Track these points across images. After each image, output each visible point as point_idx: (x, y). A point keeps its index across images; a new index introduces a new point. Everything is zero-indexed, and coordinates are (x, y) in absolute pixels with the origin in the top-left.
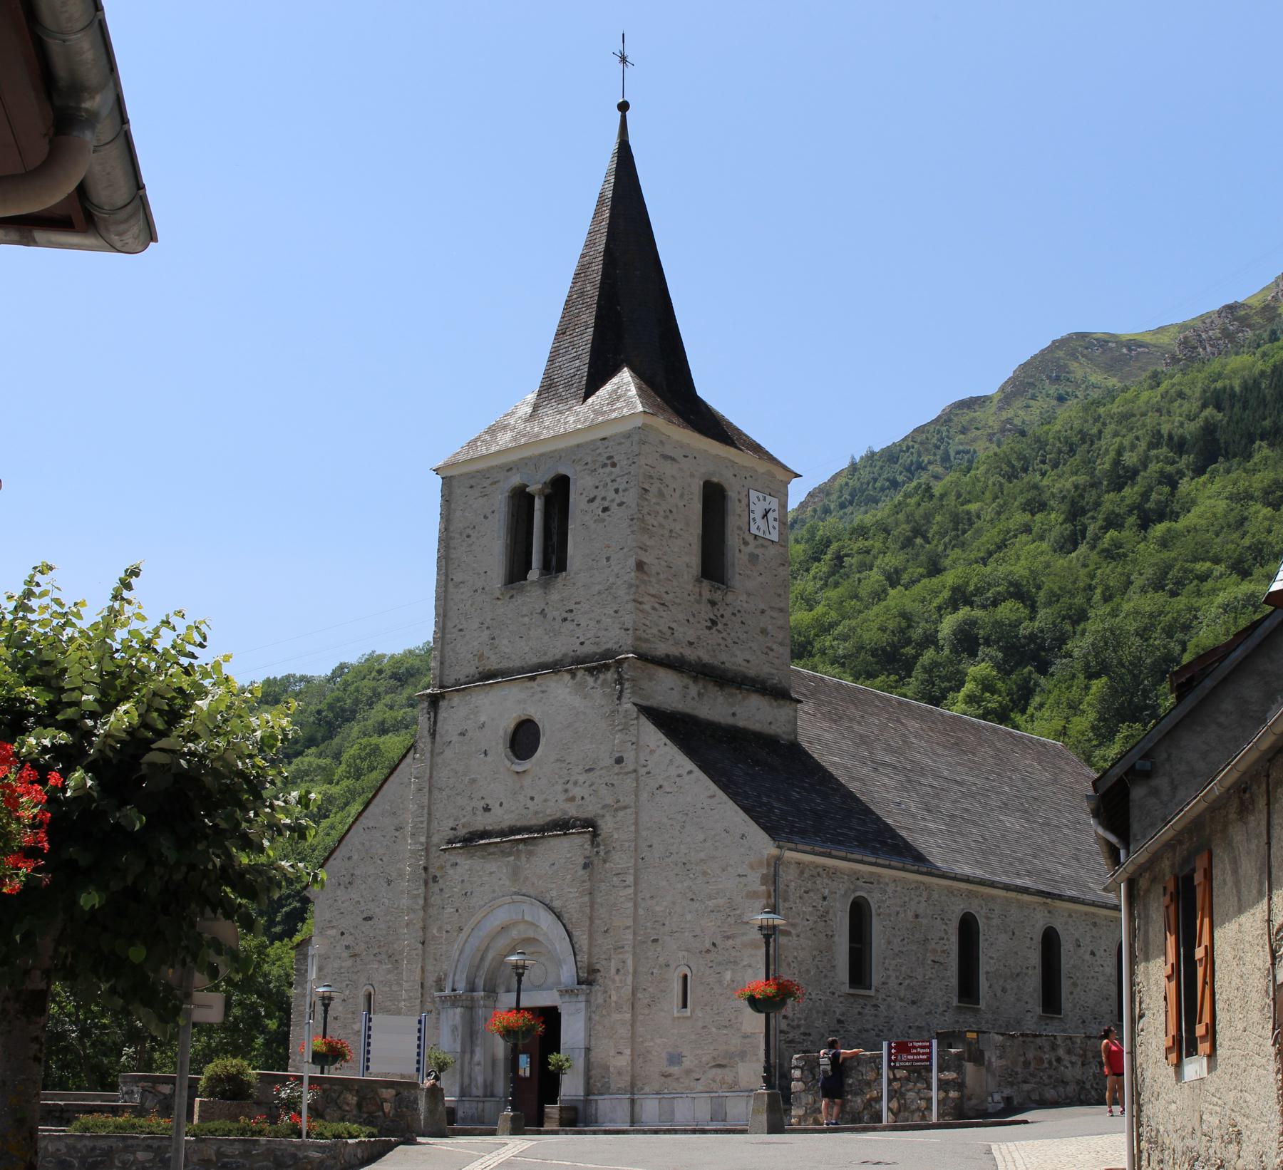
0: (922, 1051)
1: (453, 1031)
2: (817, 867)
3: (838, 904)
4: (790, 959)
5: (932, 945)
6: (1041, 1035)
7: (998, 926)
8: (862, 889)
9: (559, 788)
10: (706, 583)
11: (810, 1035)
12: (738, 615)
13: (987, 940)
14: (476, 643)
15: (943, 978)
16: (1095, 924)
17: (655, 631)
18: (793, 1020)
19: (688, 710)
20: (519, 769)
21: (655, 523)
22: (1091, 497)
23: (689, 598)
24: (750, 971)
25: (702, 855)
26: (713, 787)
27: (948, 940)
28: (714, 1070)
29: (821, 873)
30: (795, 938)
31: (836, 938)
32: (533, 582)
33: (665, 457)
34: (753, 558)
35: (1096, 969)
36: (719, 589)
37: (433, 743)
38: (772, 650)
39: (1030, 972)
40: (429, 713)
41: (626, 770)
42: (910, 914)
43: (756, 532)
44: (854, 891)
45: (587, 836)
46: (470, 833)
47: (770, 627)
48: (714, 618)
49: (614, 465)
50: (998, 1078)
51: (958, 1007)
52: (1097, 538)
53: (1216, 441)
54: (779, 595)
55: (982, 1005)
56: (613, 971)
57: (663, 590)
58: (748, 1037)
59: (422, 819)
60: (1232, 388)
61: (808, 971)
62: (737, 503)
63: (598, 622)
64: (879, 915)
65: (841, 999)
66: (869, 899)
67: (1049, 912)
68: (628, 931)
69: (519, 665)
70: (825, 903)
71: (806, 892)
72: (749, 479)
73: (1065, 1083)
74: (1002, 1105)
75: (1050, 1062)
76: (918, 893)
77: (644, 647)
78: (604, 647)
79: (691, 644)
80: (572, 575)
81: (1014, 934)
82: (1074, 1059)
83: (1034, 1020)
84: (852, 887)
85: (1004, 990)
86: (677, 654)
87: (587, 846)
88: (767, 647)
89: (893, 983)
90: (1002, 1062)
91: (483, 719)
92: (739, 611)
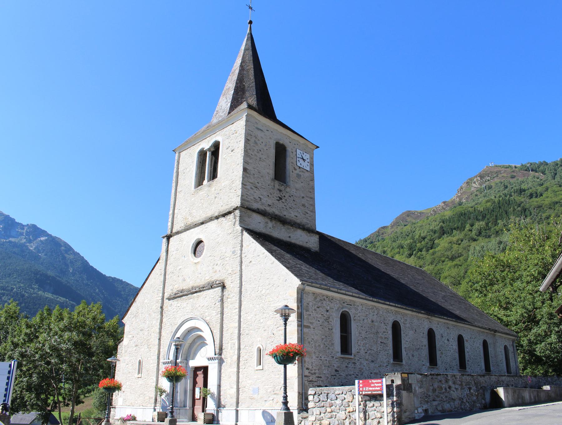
0: (377, 385)
2: (323, 296)
3: (334, 314)
4: (310, 340)
5: (380, 335)
6: (440, 375)
7: (409, 327)
8: (346, 307)
10: (276, 182)
11: (321, 377)
12: (292, 197)
13: (404, 333)
14: (184, 214)
15: (386, 350)
16: (448, 328)
17: (252, 198)
19: (267, 233)
21: (253, 154)
22: (414, 244)
23: (268, 187)
26: (273, 259)
27: (387, 333)
30: (312, 329)
31: (334, 330)
33: (258, 129)
34: (299, 176)
35: (450, 347)
36: (283, 185)
38: (308, 213)
39: (423, 348)
42: (370, 321)
43: (300, 166)
44: (342, 308)
45: (220, 288)
47: (306, 204)
48: (281, 197)
50: (420, 399)
51: (393, 363)
52: (416, 254)
53: (444, 230)
54: (310, 192)
55: (404, 362)
57: (256, 182)
60: (446, 218)
61: (319, 346)
62: (291, 153)
64: (355, 320)
65: (337, 360)
66: (350, 313)
67: (430, 322)
70: (328, 313)
71: (318, 308)
72: (296, 145)
73: (454, 400)
74: (423, 414)
75: (446, 389)
76: (372, 311)
77: (247, 204)
79: (269, 205)
81: (416, 331)
82: (457, 386)
83: (426, 369)
84: (341, 306)
85: (413, 356)
86: (263, 209)
88: (305, 212)
89: (362, 352)
90: (421, 390)
92: (292, 196)
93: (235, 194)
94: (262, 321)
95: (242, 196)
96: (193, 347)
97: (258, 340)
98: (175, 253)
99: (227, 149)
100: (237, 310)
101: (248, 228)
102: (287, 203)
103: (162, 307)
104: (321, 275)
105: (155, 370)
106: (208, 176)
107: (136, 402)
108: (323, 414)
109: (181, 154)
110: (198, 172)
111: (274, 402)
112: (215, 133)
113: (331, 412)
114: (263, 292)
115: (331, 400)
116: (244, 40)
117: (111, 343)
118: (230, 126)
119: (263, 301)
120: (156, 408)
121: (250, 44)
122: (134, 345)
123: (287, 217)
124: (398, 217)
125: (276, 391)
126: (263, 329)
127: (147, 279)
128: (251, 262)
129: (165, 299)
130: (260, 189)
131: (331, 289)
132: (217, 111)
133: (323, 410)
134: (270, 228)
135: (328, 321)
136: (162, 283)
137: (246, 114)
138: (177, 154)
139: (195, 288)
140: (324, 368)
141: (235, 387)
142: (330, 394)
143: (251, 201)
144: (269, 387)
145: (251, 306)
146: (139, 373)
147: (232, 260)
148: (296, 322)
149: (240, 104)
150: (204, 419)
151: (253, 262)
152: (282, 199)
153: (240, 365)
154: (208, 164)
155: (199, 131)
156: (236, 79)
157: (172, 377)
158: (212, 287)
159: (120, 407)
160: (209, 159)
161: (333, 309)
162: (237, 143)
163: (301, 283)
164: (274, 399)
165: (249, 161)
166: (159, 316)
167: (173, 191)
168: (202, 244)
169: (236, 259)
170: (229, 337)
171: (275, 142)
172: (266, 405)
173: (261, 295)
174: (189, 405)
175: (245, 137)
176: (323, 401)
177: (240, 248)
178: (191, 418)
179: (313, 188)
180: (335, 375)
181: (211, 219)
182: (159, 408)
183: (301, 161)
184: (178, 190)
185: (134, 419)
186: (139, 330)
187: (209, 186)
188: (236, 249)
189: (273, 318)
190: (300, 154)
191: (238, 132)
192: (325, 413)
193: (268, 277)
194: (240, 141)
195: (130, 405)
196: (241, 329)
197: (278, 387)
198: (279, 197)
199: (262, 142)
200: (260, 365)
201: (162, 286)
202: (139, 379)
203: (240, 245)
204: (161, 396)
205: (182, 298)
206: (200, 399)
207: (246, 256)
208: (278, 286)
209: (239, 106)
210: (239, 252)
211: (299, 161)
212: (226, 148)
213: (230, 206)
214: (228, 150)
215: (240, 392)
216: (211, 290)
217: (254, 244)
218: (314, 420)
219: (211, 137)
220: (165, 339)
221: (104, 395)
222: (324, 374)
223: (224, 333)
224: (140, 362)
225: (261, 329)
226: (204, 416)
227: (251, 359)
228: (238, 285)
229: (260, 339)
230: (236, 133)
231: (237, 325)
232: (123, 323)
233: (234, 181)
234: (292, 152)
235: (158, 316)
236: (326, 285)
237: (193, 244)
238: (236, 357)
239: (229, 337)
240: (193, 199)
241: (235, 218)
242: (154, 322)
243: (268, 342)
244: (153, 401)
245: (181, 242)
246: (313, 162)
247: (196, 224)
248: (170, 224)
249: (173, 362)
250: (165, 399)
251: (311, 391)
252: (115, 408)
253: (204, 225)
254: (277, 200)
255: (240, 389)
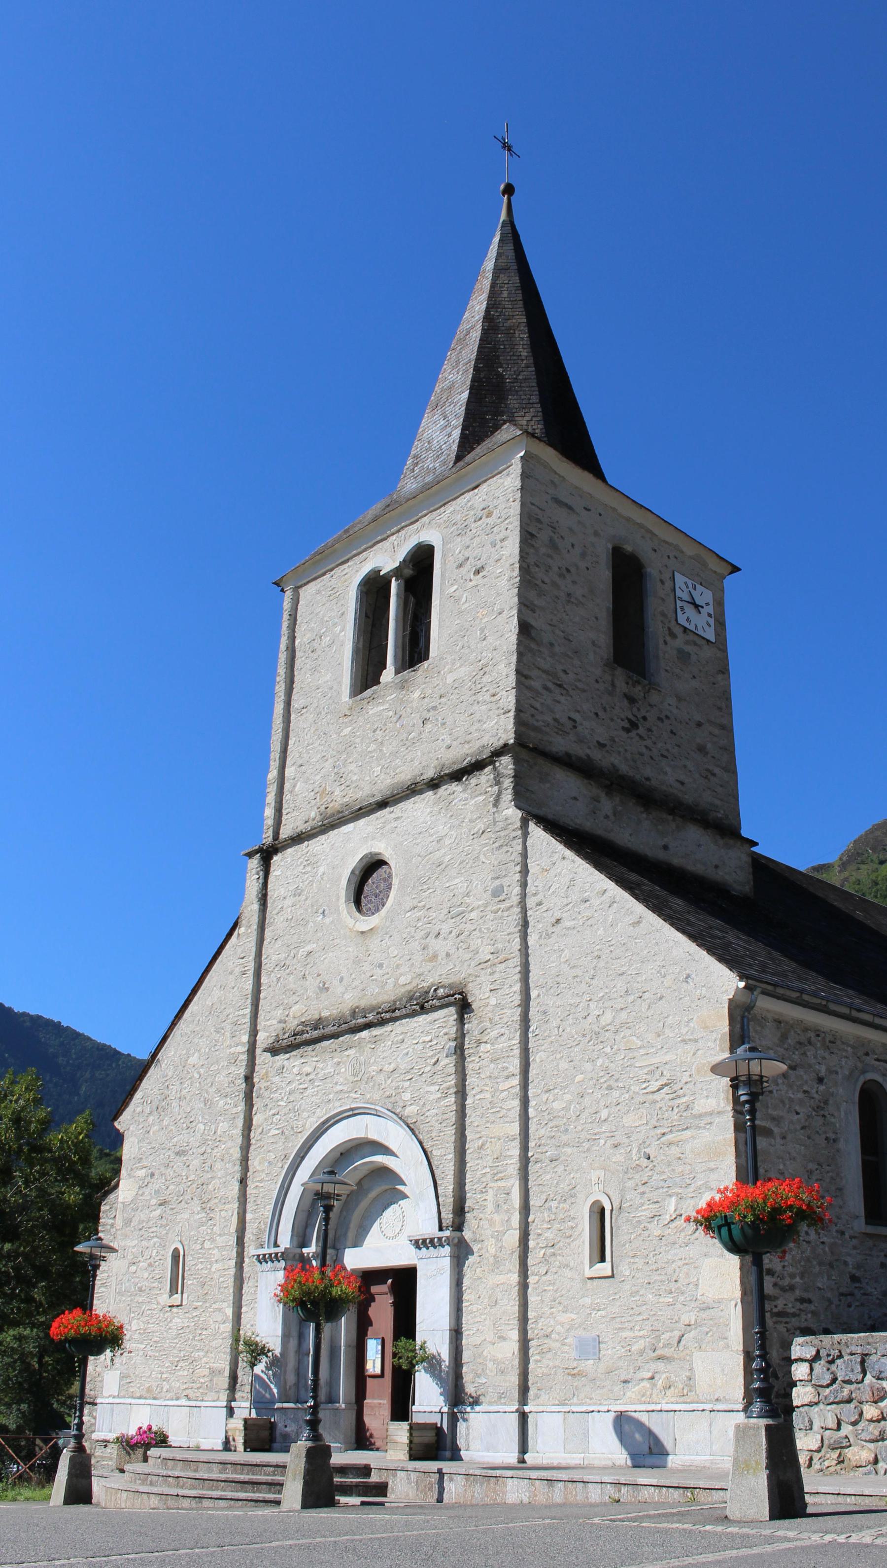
2: (806, 1030)
10: (619, 671)
11: (809, 1301)
12: (666, 722)
14: (318, 777)
17: (549, 719)
18: (782, 1278)
19: (600, 832)
20: (365, 928)
21: (546, 580)
26: (639, 908)
29: (813, 1039)
31: (841, 1145)
34: (683, 657)
36: (639, 683)
38: (714, 775)
43: (687, 625)
44: (864, 1072)
45: (452, 1009)
47: (709, 746)
48: (633, 719)
54: (720, 709)
56: (490, 1207)
62: (659, 584)
65: (854, 1241)
68: (513, 1144)
70: (822, 1088)
79: (601, 745)
88: (707, 770)
92: (667, 717)
93: (494, 706)
94: (604, 1114)
95: (519, 710)
96: (357, 1206)
97: (594, 1179)
98: (288, 902)
99: (461, 566)
100: (516, 1081)
101: (541, 813)
102: (654, 738)
103: (249, 1079)
104: (788, 965)
105: (231, 1282)
106: (395, 656)
107: (166, 1386)
108: (851, 1427)
109: (302, 591)
110: (361, 645)
111: (655, 1385)
112: (417, 521)
113: (878, 1421)
114: (604, 1020)
115: (879, 1379)
116: (490, 243)
117: (73, 1196)
118: (468, 496)
119: (608, 1050)
120: (233, 1404)
121: (511, 254)
122: (154, 1202)
123: (654, 783)
124: (861, 837)
125: (665, 1346)
126: (610, 1142)
127: (194, 991)
128: (558, 921)
129: (258, 1051)
130: (571, 692)
131: (833, 1007)
132: (416, 457)
133: (848, 1412)
134: (607, 817)
135: (822, 1112)
136: (249, 1001)
137: (522, 454)
138: (289, 594)
139: (364, 1012)
140: (817, 1269)
141: (515, 1335)
142: (873, 1358)
143: (547, 729)
144: (637, 1333)
145: (564, 1065)
146: (173, 1290)
147: (491, 916)
148: (731, 1114)
149: (493, 433)
150: (411, 1442)
151: (567, 923)
152: (638, 728)
153: (530, 1262)
154: (397, 616)
155: (357, 521)
156: (474, 356)
157: (314, 1303)
158: (422, 1007)
159: (111, 1400)
160: (398, 601)
161: (837, 1073)
162: (494, 545)
163: (742, 985)
164: (657, 1377)
165: (536, 602)
166: (241, 1107)
167: (279, 708)
168: (381, 872)
169: (506, 914)
170: (488, 1170)
171: (610, 546)
172: (629, 1394)
173: (597, 1030)
174: (345, 1395)
175: (521, 526)
176: (849, 1382)
177: (518, 877)
178: (353, 1440)
179: (726, 696)
180: (851, 1294)
181: (412, 790)
182: (247, 1404)
183: (690, 611)
184: (295, 704)
185: (162, 1440)
186: (170, 1153)
187: (403, 688)
188: (506, 882)
189: (647, 1105)
190: (684, 587)
191: (496, 513)
192: (854, 1424)
193: (623, 969)
194: (502, 540)
195: (144, 1393)
196: (532, 1144)
197: (668, 1334)
198: (630, 721)
199: (573, 545)
200: (603, 1259)
201: (248, 1011)
202: (175, 1310)
203: (518, 868)
204: (253, 1365)
205: (318, 1046)
206: (382, 1375)
207: (540, 904)
208: (661, 998)
209: (488, 437)
210: (517, 890)
211: (682, 608)
212: (455, 565)
213: (478, 744)
214: (463, 570)
215: (531, 1352)
216: (422, 1019)
217: (565, 862)
218: (815, 1447)
219: (403, 532)
220: (261, 1181)
221: (16, 1357)
222: (820, 1289)
223: (468, 1158)
224: (176, 1256)
225: (602, 1142)
226: (411, 1434)
227: (568, 1240)
228: (517, 999)
229: (601, 1173)
230: (489, 515)
231: (515, 1129)
232: (118, 1131)
233: (486, 665)
234: (662, 582)
235: (236, 1106)
236: (815, 994)
237: (353, 872)
238: (513, 1237)
239: (488, 1170)
240: (347, 731)
241: (498, 783)
242: (223, 1126)
243: (630, 1184)
244: (224, 1382)
245: (309, 869)
246: (723, 614)
247: (360, 809)
248: (269, 812)
249: (291, 1256)
250: (265, 1377)
251: (801, 1348)
252: (96, 1404)
253: (388, 809)
254: (623, 728)
255: (531, 1344)
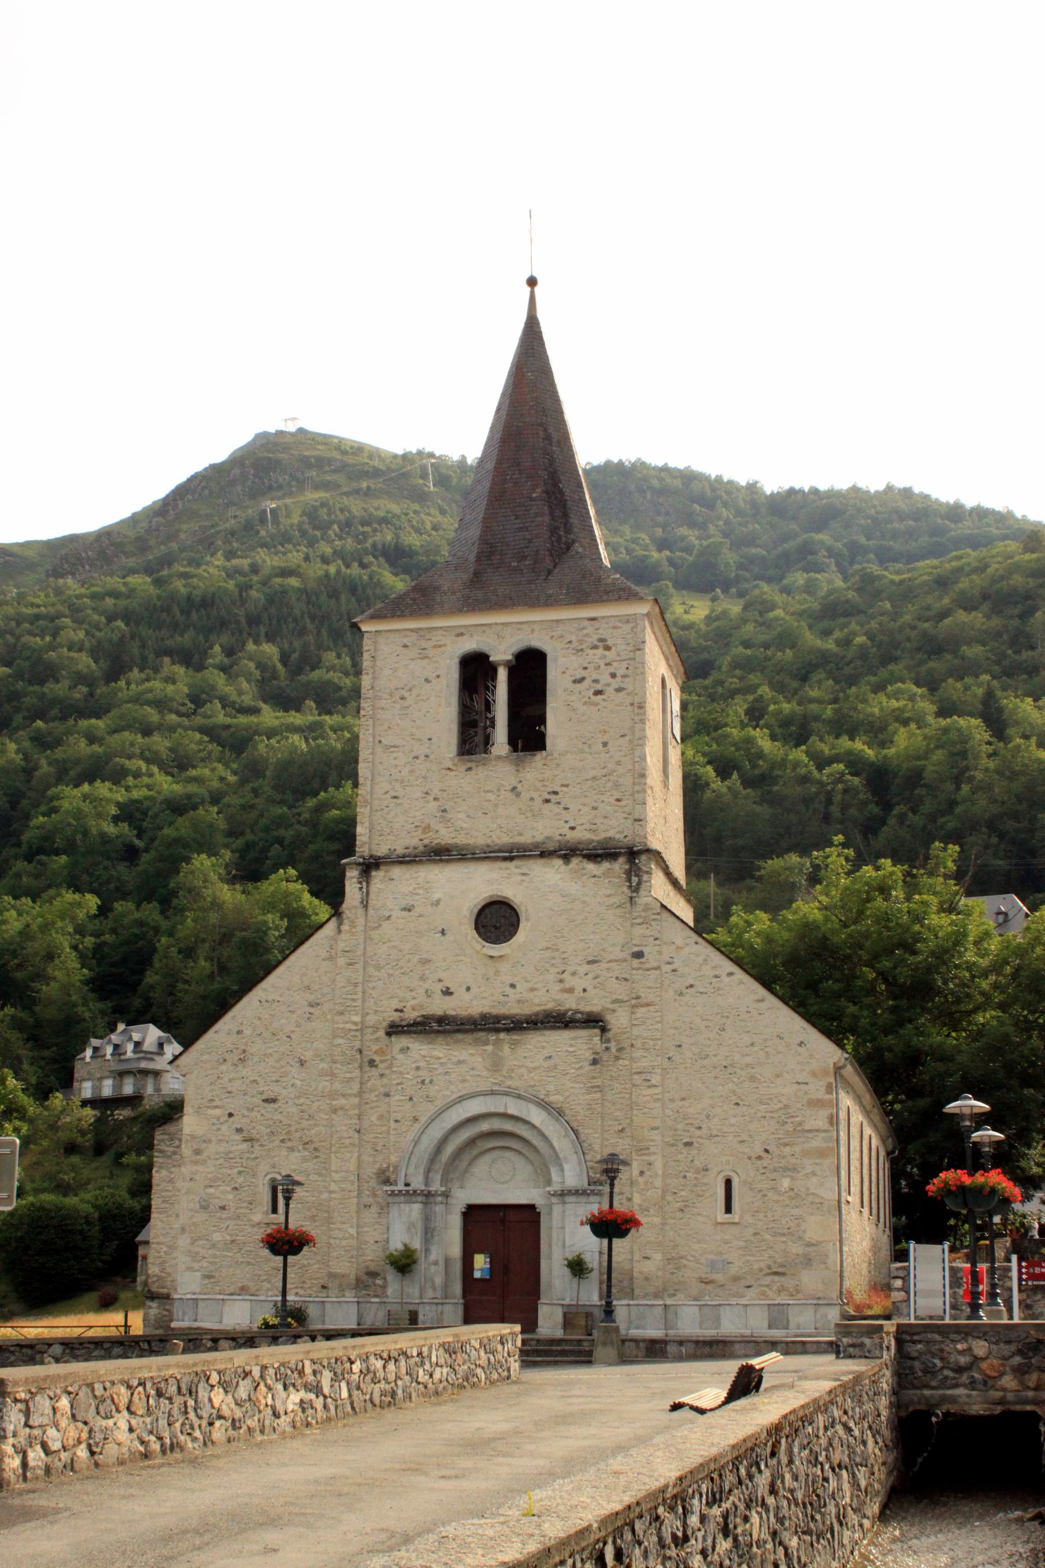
1: (409, 1228)
9: (551, 977)
14: (419, 814)
24: (814, 1179)
25: (748, 1060)
28: (770, 1278)
32: (499, 757)
37: (366, 915)
40: (360, 883)
41: (647, 966)
46: (423, 1016)
49: (608, 648)
58: (813, 1245)
59: (355, 997)
63: (595, 808)
69: (483, 842)
78: (602, 836)
80: (556, 755)
87: (597, 1039)
91: (436, 896)
